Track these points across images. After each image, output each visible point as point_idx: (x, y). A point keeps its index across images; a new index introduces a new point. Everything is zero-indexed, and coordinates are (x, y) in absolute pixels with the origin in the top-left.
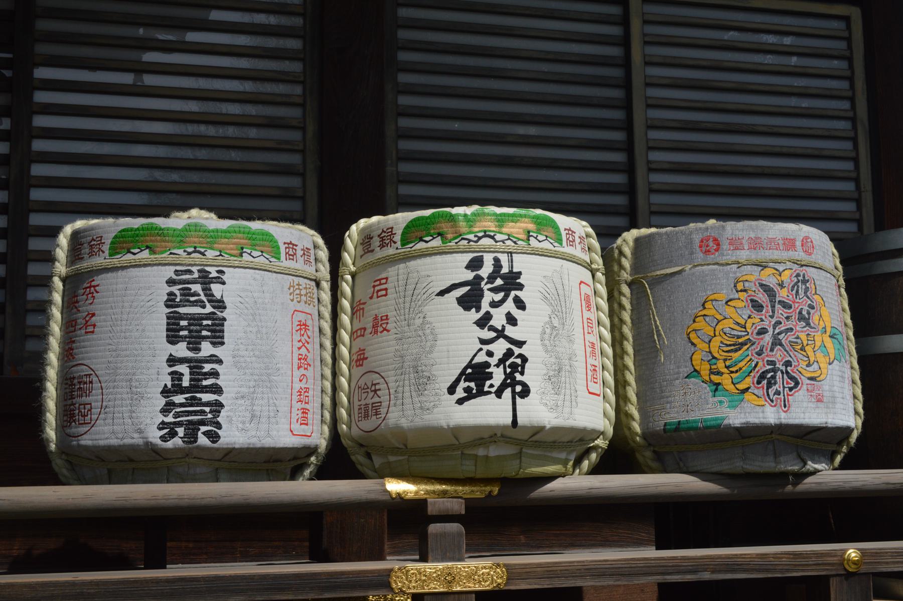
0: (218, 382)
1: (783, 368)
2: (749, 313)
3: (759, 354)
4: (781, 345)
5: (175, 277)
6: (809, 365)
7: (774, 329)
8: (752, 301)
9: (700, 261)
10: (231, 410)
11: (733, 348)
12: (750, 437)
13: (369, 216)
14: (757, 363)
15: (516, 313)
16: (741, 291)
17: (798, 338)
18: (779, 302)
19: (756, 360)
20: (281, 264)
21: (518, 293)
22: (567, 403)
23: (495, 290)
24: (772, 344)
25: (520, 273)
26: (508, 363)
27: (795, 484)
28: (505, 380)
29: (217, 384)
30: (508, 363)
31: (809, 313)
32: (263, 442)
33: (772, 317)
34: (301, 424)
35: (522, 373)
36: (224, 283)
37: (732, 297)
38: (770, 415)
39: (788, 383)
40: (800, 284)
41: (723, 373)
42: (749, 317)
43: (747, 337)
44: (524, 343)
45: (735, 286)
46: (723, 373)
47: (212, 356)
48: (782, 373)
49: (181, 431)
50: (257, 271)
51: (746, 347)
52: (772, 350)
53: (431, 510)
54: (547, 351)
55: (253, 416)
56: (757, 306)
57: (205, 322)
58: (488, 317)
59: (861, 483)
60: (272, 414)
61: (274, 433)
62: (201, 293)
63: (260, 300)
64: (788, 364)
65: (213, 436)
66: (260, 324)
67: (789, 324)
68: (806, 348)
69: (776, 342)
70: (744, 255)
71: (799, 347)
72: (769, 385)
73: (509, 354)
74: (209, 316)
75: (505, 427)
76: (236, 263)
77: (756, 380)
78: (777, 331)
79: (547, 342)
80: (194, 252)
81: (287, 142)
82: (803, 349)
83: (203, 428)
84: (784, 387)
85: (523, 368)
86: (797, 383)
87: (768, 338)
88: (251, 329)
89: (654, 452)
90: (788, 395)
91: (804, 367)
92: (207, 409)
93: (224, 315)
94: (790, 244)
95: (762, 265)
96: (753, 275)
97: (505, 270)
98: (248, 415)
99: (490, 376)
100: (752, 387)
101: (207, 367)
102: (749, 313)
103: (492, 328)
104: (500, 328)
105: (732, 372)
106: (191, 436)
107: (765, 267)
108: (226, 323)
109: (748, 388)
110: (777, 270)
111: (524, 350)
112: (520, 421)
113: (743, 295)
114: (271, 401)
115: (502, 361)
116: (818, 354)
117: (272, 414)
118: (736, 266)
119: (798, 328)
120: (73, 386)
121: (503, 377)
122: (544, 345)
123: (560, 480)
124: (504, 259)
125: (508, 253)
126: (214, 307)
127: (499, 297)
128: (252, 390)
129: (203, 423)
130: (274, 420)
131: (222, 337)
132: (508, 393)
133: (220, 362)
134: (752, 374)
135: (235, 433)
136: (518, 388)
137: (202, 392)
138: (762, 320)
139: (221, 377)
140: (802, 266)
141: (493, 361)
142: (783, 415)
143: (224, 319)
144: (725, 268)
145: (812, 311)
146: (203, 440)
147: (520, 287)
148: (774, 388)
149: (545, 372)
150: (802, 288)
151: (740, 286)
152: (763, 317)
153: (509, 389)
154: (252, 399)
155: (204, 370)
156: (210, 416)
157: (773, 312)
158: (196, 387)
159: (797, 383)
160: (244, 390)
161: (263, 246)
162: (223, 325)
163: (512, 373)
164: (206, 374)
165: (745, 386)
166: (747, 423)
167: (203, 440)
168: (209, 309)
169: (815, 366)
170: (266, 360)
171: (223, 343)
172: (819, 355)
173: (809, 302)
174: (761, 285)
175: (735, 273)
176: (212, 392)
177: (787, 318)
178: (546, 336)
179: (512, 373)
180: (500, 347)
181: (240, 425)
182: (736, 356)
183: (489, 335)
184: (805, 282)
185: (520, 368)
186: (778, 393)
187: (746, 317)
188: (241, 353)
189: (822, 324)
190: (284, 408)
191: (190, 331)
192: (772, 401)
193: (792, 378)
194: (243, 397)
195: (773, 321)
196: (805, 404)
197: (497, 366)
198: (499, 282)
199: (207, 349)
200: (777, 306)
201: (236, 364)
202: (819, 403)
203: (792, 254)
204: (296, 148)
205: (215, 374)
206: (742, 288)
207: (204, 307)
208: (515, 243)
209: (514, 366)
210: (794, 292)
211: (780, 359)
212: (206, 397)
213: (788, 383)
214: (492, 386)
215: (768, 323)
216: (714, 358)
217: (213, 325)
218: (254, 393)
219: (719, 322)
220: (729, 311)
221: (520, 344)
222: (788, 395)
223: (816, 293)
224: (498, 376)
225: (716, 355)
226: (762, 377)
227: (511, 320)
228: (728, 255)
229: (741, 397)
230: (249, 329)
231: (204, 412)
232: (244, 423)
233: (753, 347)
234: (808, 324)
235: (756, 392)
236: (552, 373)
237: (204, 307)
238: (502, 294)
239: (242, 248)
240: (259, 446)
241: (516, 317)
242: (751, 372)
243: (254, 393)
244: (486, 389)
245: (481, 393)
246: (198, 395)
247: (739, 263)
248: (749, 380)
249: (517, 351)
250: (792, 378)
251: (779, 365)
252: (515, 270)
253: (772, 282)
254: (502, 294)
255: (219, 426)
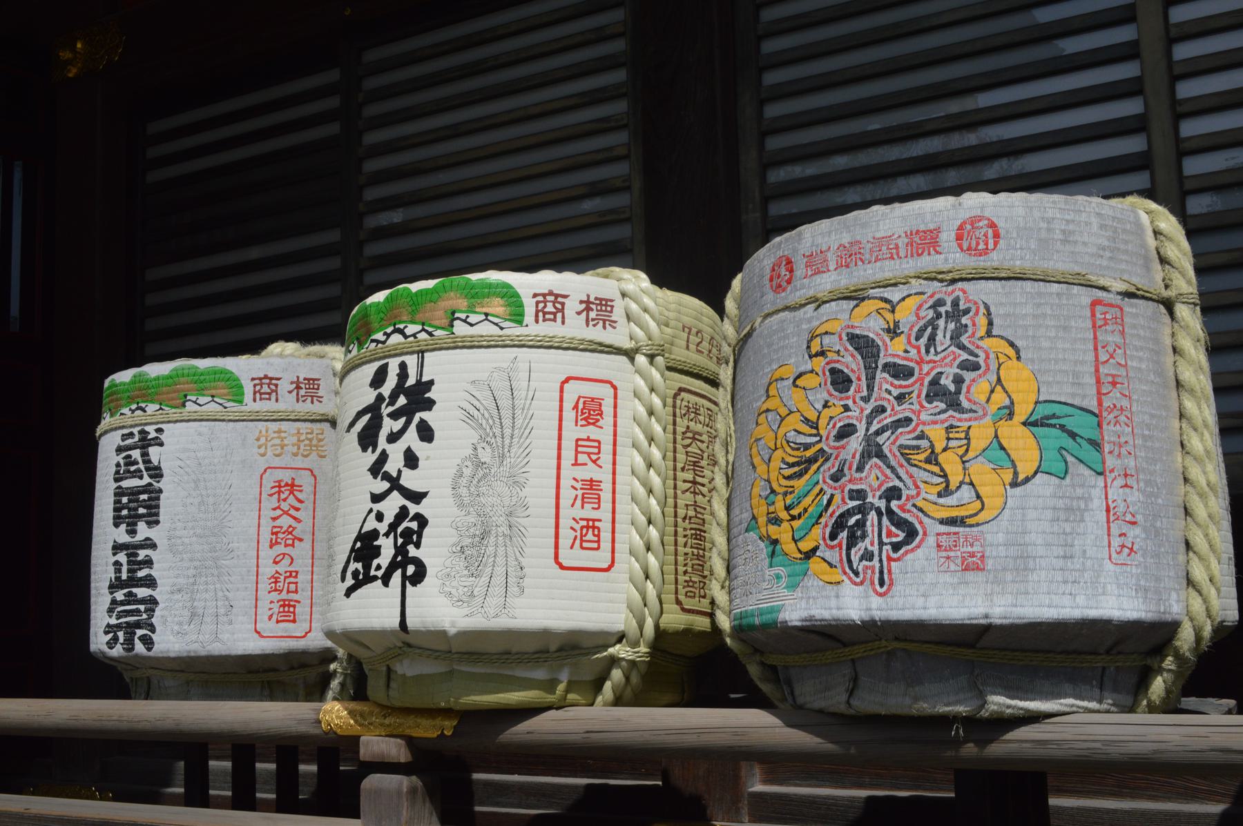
0: (153, 573)
1: (882, 504)
2: (825, 396)
3: (836, 478)
4: (880, 455)
5: (122, 444)
6: (946, 492)
7: (869, 424)
8: (833, 371)
9: (768, 308)
10: (165, 608)
11: (796, 469)
12: (854, 644)
13: (728, 287)
14: (832, 495)
15: (420, 448)
16: (816, 355)
17: (922, 436)
18: (886, 365)
19: (829, 492)
20: (243, 408)
21: (424, 415)
22: (497, 590)
23: (394, 416)
24: (862, 456)
25: (431, 383)
26: (400, 530)
27: (983, 743)
28: (395, 556)
29: (150, 575)
30: (400, 530)
31: (958, 381)
32: (209, 648)
33: (866, 400)
34: (278, 622)
35: (418, 545)
36: (161, 444)
37: (802, 369)
38: (852, 603)
39: (889, 534)
40: (941, 322)
41: (782, 521)
42: (826, 406)
43: (818, 447)
44: (424, 495)
45: (809, 347)
46: (782, 521)
47: (147, 539)
48: (879, 513)
49: (121, 634)
50: (204, 423)
51: (814, 467)
52: (860, 469)
53: (365, 753)
54: (461, 505)
55: (193, 615)
56: (840, 381)
57: (142, 497)
58: (384, 457)
59: (1155, 746)
60: (222, 611)
61: (225, 637)
62: (140, 460)
63: (207, 461)
64: (892, 494)
65: (148, 642)
66: (204, 493)
67: (903, 411)
68: (941, 458)
69: (873, 450)
70: (827, 282)
71: (922, 457)
72: (852, 541)
73: (403, 514)
74: (147, 489)
75: (393, 632)
76: (177, 417)
77: (828, 530)
78: (873, 429)
79: (464, 491)
80: (137, 409)
81: (611, 211)
82: (932, 459)
83: (139, 632)
84: (881, 544)
85: (420, 536)
86: (911, 533)
87: (855, 444)
88: (192, 500)
89: (762, 664)
90: (890, 559)
91: (934, 498)
92: (142, 607)
93: (160, 485)
94: (927, 240)
95: (856, 296)
96: (839, 316)
97: (411, 381)
98: (187, 613)
99: (377, 552)
100: (822, 547)
101: (142, 554)
102: (825, 396)
103: (387, 477)
104: (395, 475)
105: (793, 518)
106: (129, 643)
107: (863, 299)
108: (162, 496)
109: (815, 549)
110: (886, 301)
111: (422, 508)
112: (411, 623)
113: (820, 361)
114: (220, 594)
115: (393, 527)
116: (974, 467)
117: (222, 611)
118: (813, 306)
119: (924, 417)
120: (135, 574)
121: (393, 551)
122: (457, 496)
123: (552, 713)
124: (412, 361)
125: (418, 352)
126: (151, 477)
127: (397, 425)
128: (191, 580)
129: (138, 625)
130: (225, 619)
131: (157, 514)
132: (397, 577)
133: (153, 546)
134: (823, 520)
135: (173, 637)
136: (411, 570)
137: (137, 586)
138: (847, 408)
139: (155, 566)
140: (953, 281)
141: (383, 527)
142: (876, 601)
143: (160, 491)
144: (797, 313)
145: (968, 376)
146: (139, 648)
147: (429, 404)
148: (861, 546)
149: (455, 540)
150: (945, 329)
151: (815, 348)
152: (850, 402)
153: (399, 571)
154: (192, 592)
155: (139, 558)
156: (145, 616)
157: (870, 388)
158: (133, 582)
159: (911, 533)
160: (181, 581)
161: (215, 388)
162: (158, 499)
163: (404, 545)
164: (140, 563)
165: (811, 545)
166: (811, 619)
167: (139, 648)
168: (146, 480)
169: (966, 493)
170: (212, 539)
171: (157, 522)
172: (981, 471)
173: (965, 356)
174: (853, 338)
175: (809, 321)
176: (148, 586)
177: (900, 398)
178: (464, 481)
179: (404, 545)
180: (394, 503)
181: (176, 628)
182: (799, 484)
183: (381, 486)
184: (957, 313)
185: (415, 537)
186: (868, 556)
187: (819, 406)
188: (178, 533)
189: (999, 398)
190: (243, 600)
191: (130, 510)
192: (857, 574)
193: (900, 523)
194: (179, 591)
195: (869, 408)
196: (929, 578)
197: (387, 535)
198: (402, 401)
199: (143, 531)
200: (880, 375)
201: (172, 549)
202: (970, 576)
203: (928, 262)
204: (622, 216)
205: (148, 563)
206: (818, 348)
207: (141, 478)
208: (430, 334)
209: (407, 534)
210: (923, 341)
211: (876, 484)
212: (141, 592)
213: (889, 534)
214: (379, 567)
215: (856, 416)
216: (773, 491)
217: (150, 499)
218: (194, 584)
219: (782, 419)
220: (795, 398)
221: (417, 497)
222: (890, 559)
223: (989, 334)
224: (387, 548)
225: (775, 486)
226: (839, 525)
227: (411, 460)
228: (803, 287)
229: (805, 566)
230: (189, 501)
231: (138, 611)
232: (180, 624)
233: (829, 464)
234: (954, 405)
235: (828, 555)
236: (467, 541)
237: (141, 478)
238: (403, 420)
239: (186, 396)
240: (203, 653)
241: (418, 454)
242: (821, 516)
243: (194, 584)
244: (373, 573)
245: (369, 579)
246: (134, 590)
247: (817, 300)
248: (817, 532)
249: (413, 509)
250: (900, 523)
251: (874, 499)
252: (424, 379)
253: (870, 324)
254: (403, 420)
255: (152, 629)
